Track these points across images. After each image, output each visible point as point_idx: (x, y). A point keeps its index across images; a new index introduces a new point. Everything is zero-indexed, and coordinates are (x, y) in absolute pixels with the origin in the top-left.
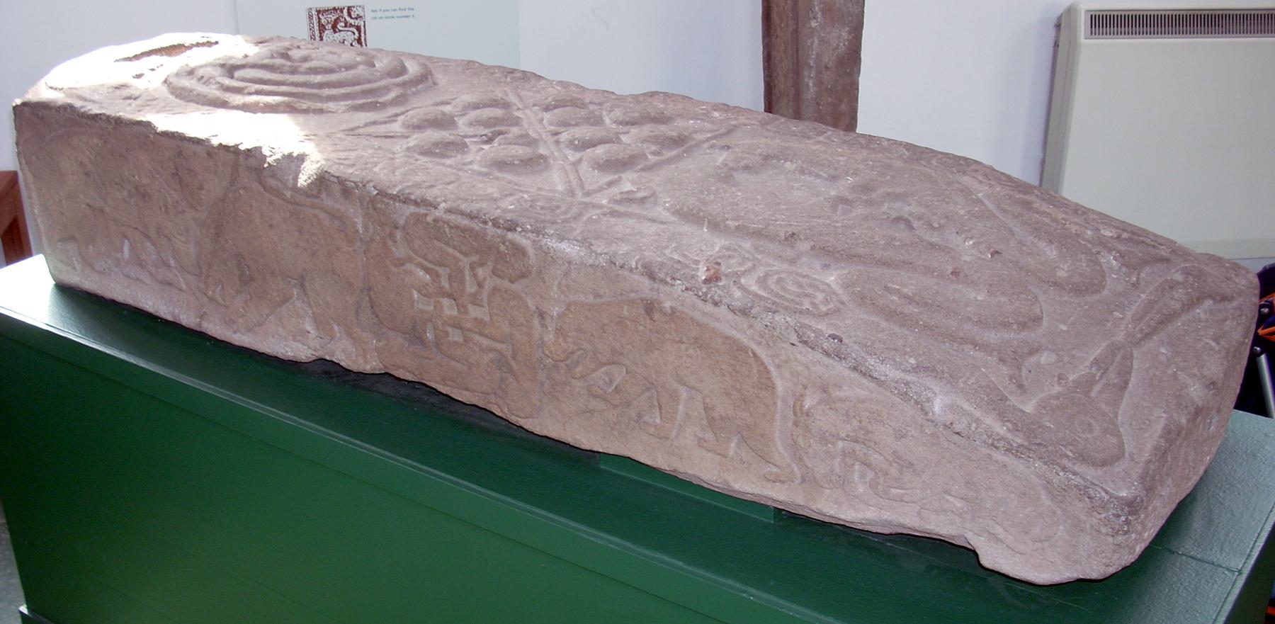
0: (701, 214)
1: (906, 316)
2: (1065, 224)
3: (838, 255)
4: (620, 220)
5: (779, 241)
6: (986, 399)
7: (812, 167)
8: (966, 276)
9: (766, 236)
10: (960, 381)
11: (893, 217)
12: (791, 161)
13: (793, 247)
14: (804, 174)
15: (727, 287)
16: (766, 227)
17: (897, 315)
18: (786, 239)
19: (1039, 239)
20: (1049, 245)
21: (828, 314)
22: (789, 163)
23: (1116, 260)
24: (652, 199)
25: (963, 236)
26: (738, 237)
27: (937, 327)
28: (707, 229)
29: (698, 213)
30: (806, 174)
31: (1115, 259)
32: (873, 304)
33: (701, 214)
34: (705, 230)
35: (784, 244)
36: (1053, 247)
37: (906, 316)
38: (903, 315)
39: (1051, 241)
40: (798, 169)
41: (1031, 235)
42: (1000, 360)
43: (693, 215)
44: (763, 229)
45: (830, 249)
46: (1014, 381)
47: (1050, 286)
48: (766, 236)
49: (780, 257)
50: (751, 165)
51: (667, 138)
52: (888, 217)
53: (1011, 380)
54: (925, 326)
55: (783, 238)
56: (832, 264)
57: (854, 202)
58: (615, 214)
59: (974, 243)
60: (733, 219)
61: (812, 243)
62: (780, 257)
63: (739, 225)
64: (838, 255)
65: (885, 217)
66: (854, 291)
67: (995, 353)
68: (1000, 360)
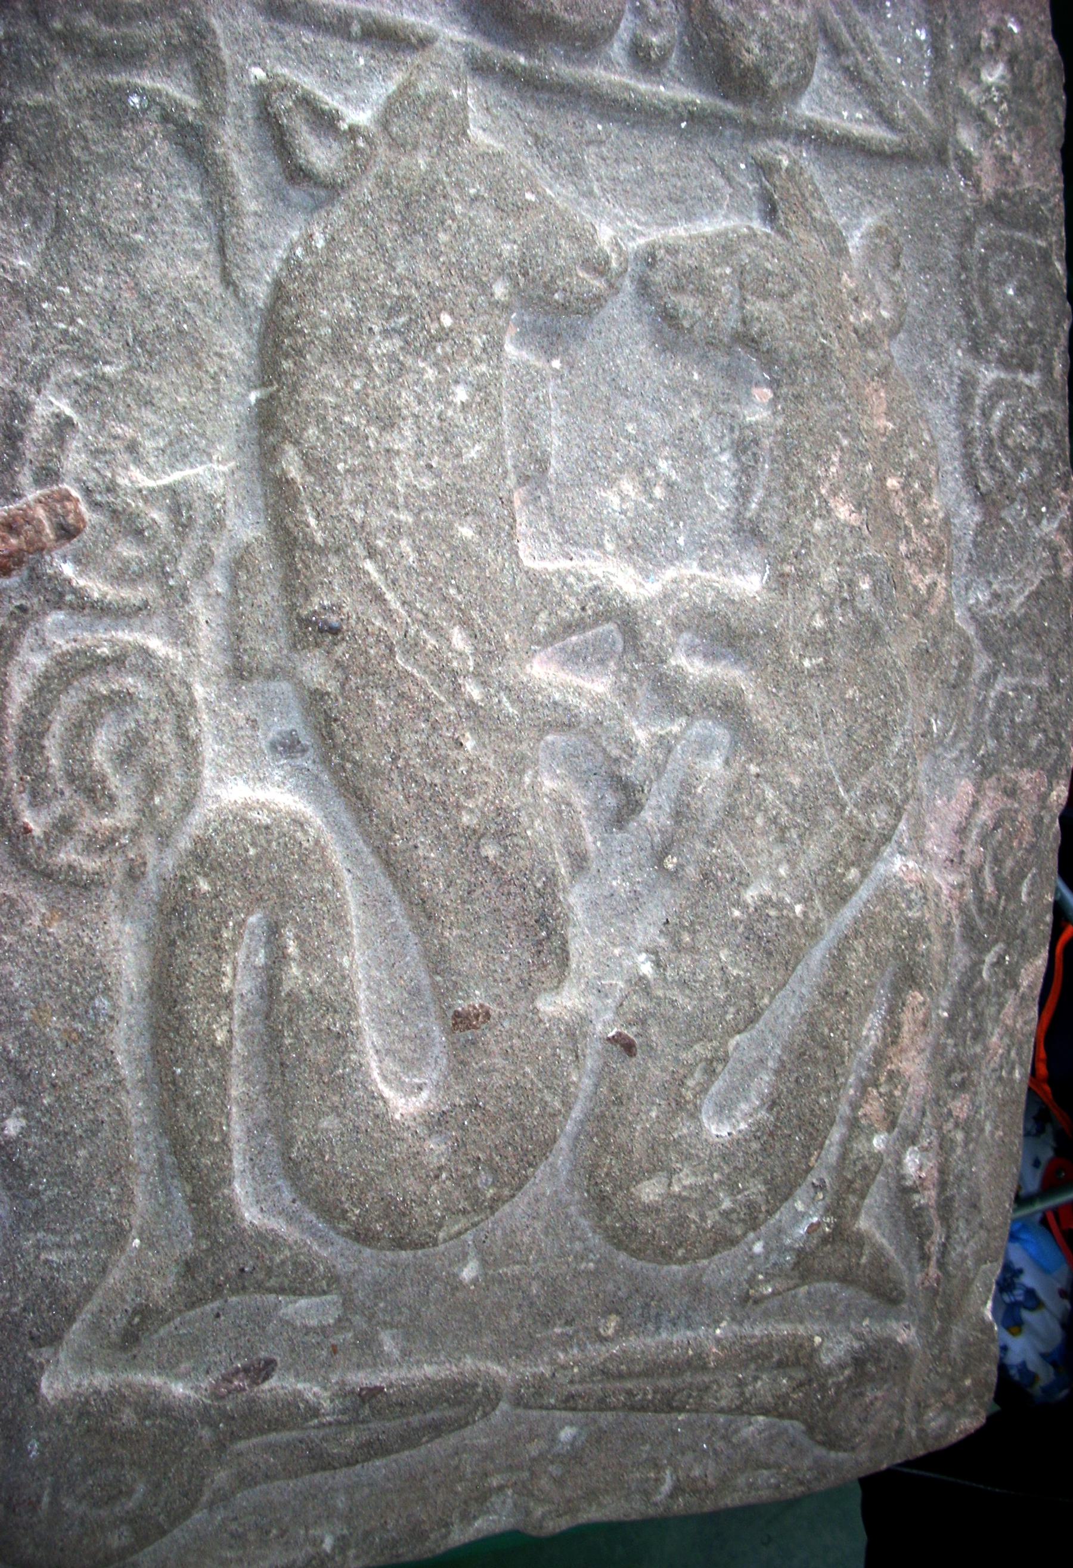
0: (287, 365)
1: (177, 1030)
2: (876, 1086)
3: (336, 760)
4: (178, 164)
5: (293, 607)
6: (15, 1310)
7: (774, 460)
8: (474, 1043)
9: (291, 566)
10: (40, 1235)
11: (624, 771)
12: (776, 397)
13: (295, 646)
14: (736, 456)
15: (483, 382)
16: (322, 551)
17: (170, 1011)
18: (305, 622)
19: (777, 1072)
20: (763, 1104)
21: (49, 876)
22: (770, 395)
23: (808, 1232)
24: (323, 193)
25: (662, 941)
26: (265, 494)
27: (189, 1107)
28: (259, 401)
29: (287, 356)
30: (739, 460)
31: (813, 1228)
32: (173, 943)
33: (287, 365)
34: (253, 397)
35: (291, 624)
36: (763, 1114)
37: (177, 1030)
38: (176, 1023)
39: (774, 1103)
40: (748, 432)
41: (784, 1049)
42: (187, 1263)
43: (278, 345)
44: (312, 546)
45: (341, 736)
46: (137, 1320)
47: (588, 1191)
48: (291, 566)
49: (238, 637)
50: (686, 324)
51: (724, 48)
52: (617, 760)
53: (135, 1312)
54: (174, 1083)
55: (304, 613)
56: (310, 753)
57: (637, 652)
58: (190, 140)
59: (642, 978)
60: (304, 456)
61: (332, 687)
62: (238, 637)
63: (290, 482)
64: (336, 760)
65: (615, 752)
66: (191, 880)
67: (204, 1244)
68: (187, 1263)
